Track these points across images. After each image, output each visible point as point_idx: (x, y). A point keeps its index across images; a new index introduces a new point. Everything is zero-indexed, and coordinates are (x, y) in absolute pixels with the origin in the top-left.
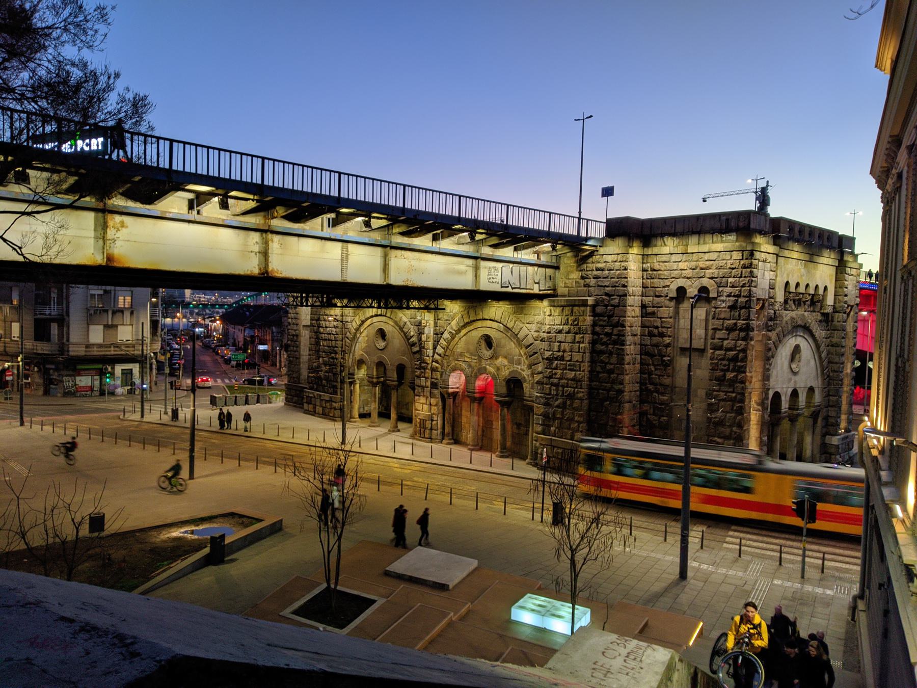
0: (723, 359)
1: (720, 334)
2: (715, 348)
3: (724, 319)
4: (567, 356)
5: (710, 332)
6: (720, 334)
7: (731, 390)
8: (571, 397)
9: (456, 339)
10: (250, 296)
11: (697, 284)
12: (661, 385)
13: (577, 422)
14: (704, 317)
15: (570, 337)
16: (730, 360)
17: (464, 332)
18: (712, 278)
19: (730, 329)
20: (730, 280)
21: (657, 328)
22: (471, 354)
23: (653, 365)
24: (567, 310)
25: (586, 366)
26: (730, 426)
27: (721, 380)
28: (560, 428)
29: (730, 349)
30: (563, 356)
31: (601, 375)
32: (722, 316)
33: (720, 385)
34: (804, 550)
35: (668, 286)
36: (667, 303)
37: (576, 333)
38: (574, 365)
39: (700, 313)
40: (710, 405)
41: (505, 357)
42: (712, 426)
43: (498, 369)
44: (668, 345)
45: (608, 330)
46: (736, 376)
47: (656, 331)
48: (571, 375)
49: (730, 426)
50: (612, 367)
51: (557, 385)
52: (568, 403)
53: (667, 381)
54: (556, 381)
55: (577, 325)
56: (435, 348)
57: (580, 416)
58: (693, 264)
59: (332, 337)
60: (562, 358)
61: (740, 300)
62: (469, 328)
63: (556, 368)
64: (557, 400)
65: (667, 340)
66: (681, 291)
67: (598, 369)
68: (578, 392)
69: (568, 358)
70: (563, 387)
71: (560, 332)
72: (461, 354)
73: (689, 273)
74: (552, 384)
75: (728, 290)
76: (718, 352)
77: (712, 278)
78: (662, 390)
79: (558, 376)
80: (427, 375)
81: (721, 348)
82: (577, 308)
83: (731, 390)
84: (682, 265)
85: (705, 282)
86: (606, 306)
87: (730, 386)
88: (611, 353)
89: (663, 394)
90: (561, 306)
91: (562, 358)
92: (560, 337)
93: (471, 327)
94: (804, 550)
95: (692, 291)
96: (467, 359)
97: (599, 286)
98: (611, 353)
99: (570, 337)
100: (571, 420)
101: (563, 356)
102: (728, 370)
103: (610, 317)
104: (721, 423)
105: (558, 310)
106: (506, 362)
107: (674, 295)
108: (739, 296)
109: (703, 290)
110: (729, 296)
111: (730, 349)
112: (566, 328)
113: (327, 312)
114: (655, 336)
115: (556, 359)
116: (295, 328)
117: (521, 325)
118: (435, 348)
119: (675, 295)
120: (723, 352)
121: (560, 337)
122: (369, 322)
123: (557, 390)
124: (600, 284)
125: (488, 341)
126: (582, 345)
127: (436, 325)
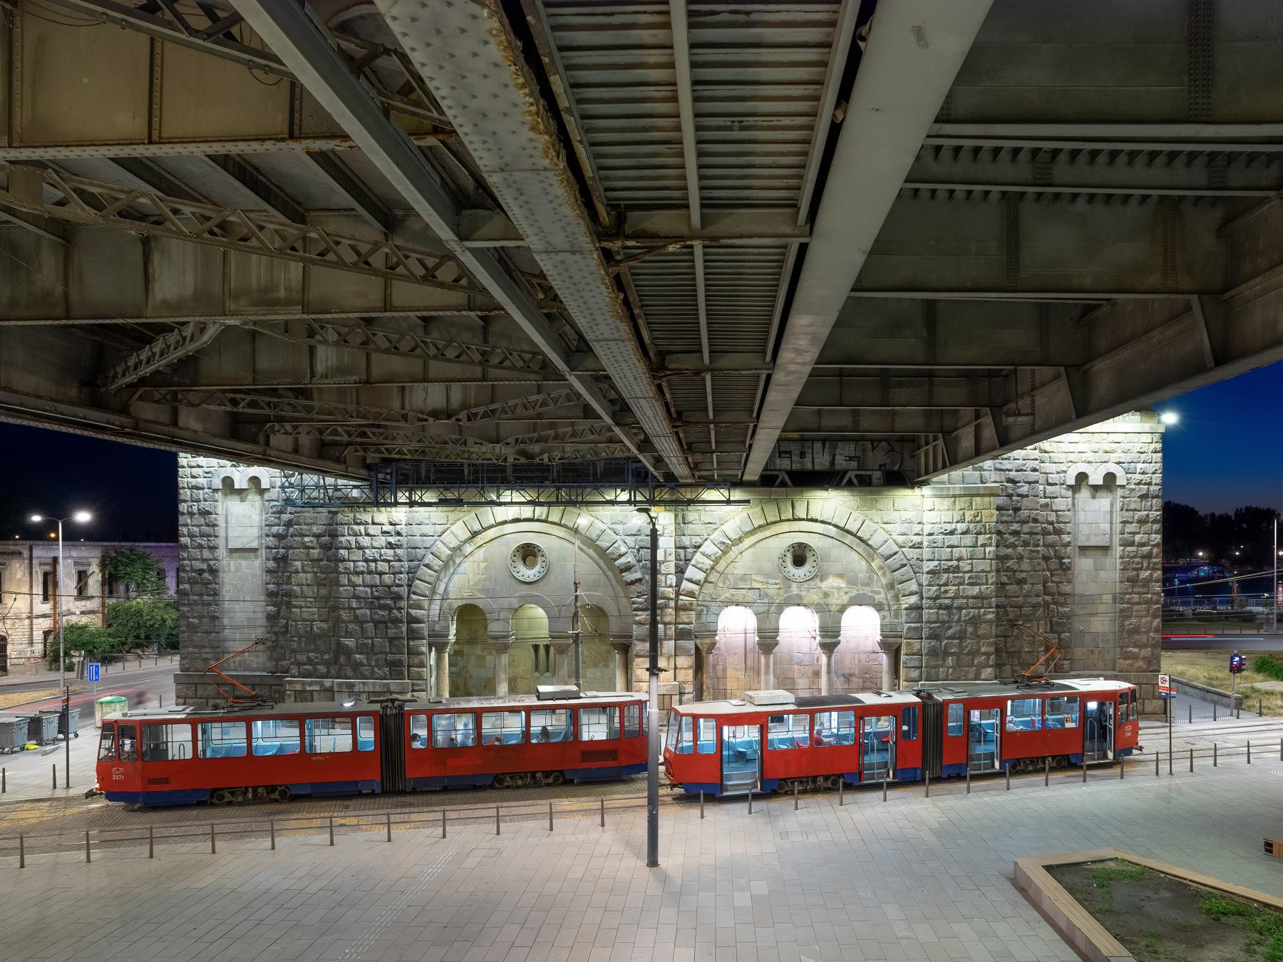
0: (1135, 557)
1: (1130, 528)
2: (1126, 544)
3: (1135, 510)
4: (965, 565)
5: (1118, 527)
6: (1130, 528)
7: (1145, 590)
8: (975, 621)
9: (732, 554)
10: (355, 487)
11: (1103, 470)
12: (1060, 594)
13: (984, 654)
14: (1108, 509)
15: (968, 540)
16: (1143, 557)
17: (748, 542)
18: (1118, 463)
19: (1142, 522)
20: (1140, 466)
21: (1052, 523)
22: (767, 576)
23: (1048, 569)
24: (962, 503)
25: (992, 578)
26: (1147, 632)
27: (1133, 581)
28: (958, 665)
29: (1143, 545)
30: (958, 567)
31: (1008, 587)
32: (1132, 507)
33: (1133, 587)
34: (212, 825)
35: (1065, 472)
36: (1064, 492)
37: (980, 533)
38: (976, 577)
39: (1104, 502)
40: (1122, 611)
41: (841, 576)
42: (1125, 635)
43: (826, 595)
44: (1068, 544)
45: (1015, 527)
46: (1151, 575)
47: (1050, 527)
48: (975, 590)
49: (1147, 632)
50: (1024, 575)
51: (947, 608)
52: (970, 629)
53: (1066, 588)
54: (947, 601)
55: (980, 521)
56: (680, 571)
57: (989, 645)
58: (1095, 447)
59: (383, 566)
60: (957, 569)
61: (1152, 488)
62: (759, 536)
63: (946, 584)
64: (950, 628)
65: (1066, 538)
66: (1082, 477)
67: (1004, 579)
68: (985, 614)
69: (968, 568)
70: (960, 608)
71: (952, 533)
72: (744, 578)
73: (1091, 457)
74: (940, 607)
75: (1138, 477)
76: (1129, 549)
77: (1118, 463)
78: (1061, 599)
79: (951, 594)
80: (667, 619)
81: (1132, 544)
82: (978, 499)
83: (1145, 590)
84: (1081, 447)
85: (1113, 468)
86: (1010, 496)
87: (1144, 586)
88: (1020, 558)
89: (1062, 605)
90: (954, 496)
91: (957, 569)
92: (954, 540)
93: (767, 533)
94: (212, 825)
95: (1096, 478)
96: (755, 585)
97: (996, 469)
98: (1020, 558)
99: (968, 540)
100: (974, 653)
101: (958, 567)
102: (1141, 569)
103: (1016, 509)
104: (1136, 631)
105: (947, 502)
106: (842, 583)
107: (1072, 481)
108: (1150, 484)
109: (1110, 477)
110: (1139, 484)
111: (1143, 545)
112: (961, 527)
113: (367, 517)
114: (1049, 534)
115: (947, 571)
116: (206, 554)
117: (876, 526)
118: (680, 571)
119: (1073, 483)
120: (1134, 548)
121: (954, 540)
122: (491, 533)
123: (950, 615)
124: (998, 466)
125: (800, 556)
126: (988, 549)
127: (680, 533)
